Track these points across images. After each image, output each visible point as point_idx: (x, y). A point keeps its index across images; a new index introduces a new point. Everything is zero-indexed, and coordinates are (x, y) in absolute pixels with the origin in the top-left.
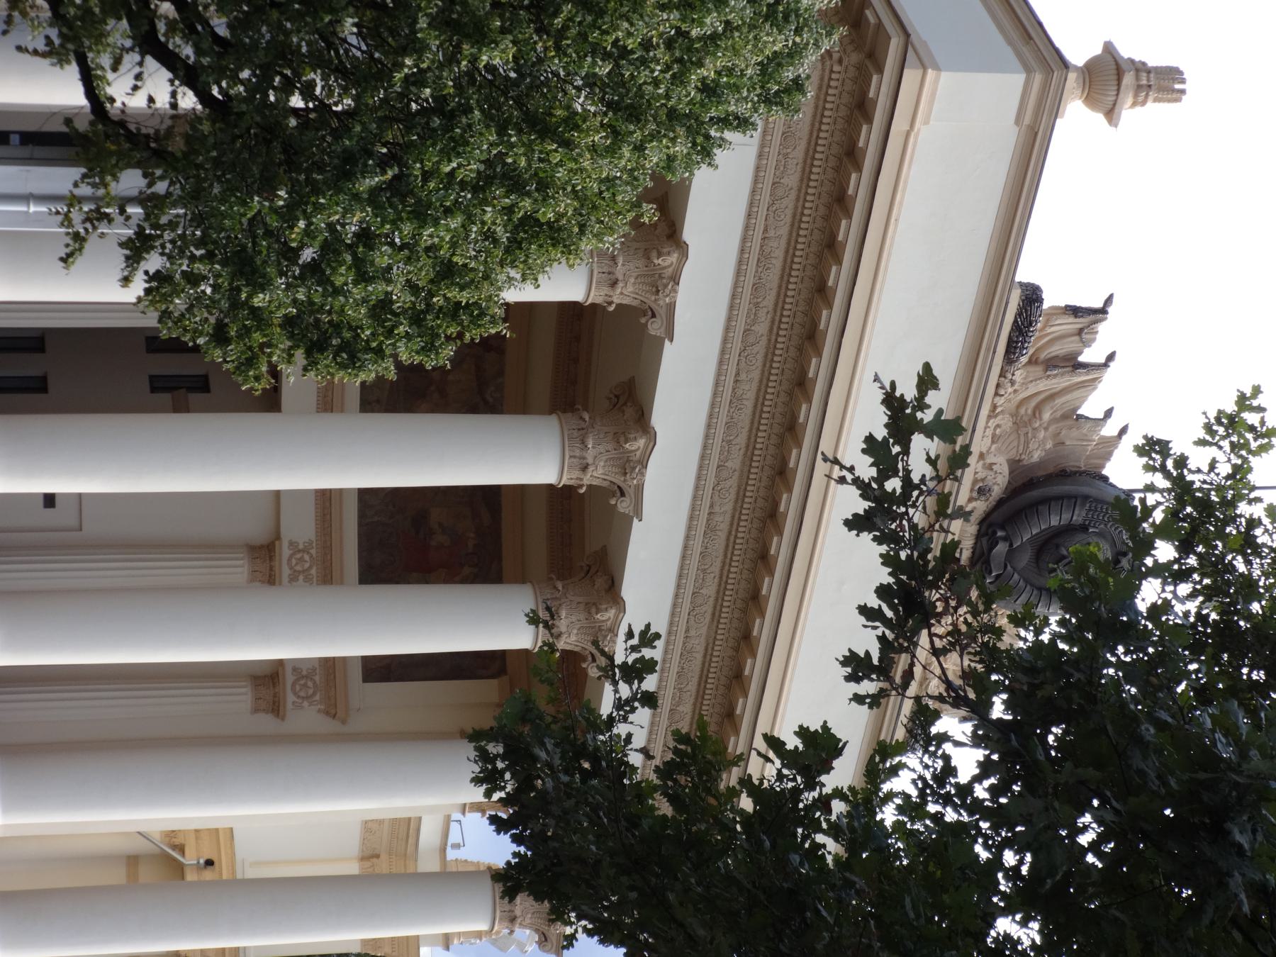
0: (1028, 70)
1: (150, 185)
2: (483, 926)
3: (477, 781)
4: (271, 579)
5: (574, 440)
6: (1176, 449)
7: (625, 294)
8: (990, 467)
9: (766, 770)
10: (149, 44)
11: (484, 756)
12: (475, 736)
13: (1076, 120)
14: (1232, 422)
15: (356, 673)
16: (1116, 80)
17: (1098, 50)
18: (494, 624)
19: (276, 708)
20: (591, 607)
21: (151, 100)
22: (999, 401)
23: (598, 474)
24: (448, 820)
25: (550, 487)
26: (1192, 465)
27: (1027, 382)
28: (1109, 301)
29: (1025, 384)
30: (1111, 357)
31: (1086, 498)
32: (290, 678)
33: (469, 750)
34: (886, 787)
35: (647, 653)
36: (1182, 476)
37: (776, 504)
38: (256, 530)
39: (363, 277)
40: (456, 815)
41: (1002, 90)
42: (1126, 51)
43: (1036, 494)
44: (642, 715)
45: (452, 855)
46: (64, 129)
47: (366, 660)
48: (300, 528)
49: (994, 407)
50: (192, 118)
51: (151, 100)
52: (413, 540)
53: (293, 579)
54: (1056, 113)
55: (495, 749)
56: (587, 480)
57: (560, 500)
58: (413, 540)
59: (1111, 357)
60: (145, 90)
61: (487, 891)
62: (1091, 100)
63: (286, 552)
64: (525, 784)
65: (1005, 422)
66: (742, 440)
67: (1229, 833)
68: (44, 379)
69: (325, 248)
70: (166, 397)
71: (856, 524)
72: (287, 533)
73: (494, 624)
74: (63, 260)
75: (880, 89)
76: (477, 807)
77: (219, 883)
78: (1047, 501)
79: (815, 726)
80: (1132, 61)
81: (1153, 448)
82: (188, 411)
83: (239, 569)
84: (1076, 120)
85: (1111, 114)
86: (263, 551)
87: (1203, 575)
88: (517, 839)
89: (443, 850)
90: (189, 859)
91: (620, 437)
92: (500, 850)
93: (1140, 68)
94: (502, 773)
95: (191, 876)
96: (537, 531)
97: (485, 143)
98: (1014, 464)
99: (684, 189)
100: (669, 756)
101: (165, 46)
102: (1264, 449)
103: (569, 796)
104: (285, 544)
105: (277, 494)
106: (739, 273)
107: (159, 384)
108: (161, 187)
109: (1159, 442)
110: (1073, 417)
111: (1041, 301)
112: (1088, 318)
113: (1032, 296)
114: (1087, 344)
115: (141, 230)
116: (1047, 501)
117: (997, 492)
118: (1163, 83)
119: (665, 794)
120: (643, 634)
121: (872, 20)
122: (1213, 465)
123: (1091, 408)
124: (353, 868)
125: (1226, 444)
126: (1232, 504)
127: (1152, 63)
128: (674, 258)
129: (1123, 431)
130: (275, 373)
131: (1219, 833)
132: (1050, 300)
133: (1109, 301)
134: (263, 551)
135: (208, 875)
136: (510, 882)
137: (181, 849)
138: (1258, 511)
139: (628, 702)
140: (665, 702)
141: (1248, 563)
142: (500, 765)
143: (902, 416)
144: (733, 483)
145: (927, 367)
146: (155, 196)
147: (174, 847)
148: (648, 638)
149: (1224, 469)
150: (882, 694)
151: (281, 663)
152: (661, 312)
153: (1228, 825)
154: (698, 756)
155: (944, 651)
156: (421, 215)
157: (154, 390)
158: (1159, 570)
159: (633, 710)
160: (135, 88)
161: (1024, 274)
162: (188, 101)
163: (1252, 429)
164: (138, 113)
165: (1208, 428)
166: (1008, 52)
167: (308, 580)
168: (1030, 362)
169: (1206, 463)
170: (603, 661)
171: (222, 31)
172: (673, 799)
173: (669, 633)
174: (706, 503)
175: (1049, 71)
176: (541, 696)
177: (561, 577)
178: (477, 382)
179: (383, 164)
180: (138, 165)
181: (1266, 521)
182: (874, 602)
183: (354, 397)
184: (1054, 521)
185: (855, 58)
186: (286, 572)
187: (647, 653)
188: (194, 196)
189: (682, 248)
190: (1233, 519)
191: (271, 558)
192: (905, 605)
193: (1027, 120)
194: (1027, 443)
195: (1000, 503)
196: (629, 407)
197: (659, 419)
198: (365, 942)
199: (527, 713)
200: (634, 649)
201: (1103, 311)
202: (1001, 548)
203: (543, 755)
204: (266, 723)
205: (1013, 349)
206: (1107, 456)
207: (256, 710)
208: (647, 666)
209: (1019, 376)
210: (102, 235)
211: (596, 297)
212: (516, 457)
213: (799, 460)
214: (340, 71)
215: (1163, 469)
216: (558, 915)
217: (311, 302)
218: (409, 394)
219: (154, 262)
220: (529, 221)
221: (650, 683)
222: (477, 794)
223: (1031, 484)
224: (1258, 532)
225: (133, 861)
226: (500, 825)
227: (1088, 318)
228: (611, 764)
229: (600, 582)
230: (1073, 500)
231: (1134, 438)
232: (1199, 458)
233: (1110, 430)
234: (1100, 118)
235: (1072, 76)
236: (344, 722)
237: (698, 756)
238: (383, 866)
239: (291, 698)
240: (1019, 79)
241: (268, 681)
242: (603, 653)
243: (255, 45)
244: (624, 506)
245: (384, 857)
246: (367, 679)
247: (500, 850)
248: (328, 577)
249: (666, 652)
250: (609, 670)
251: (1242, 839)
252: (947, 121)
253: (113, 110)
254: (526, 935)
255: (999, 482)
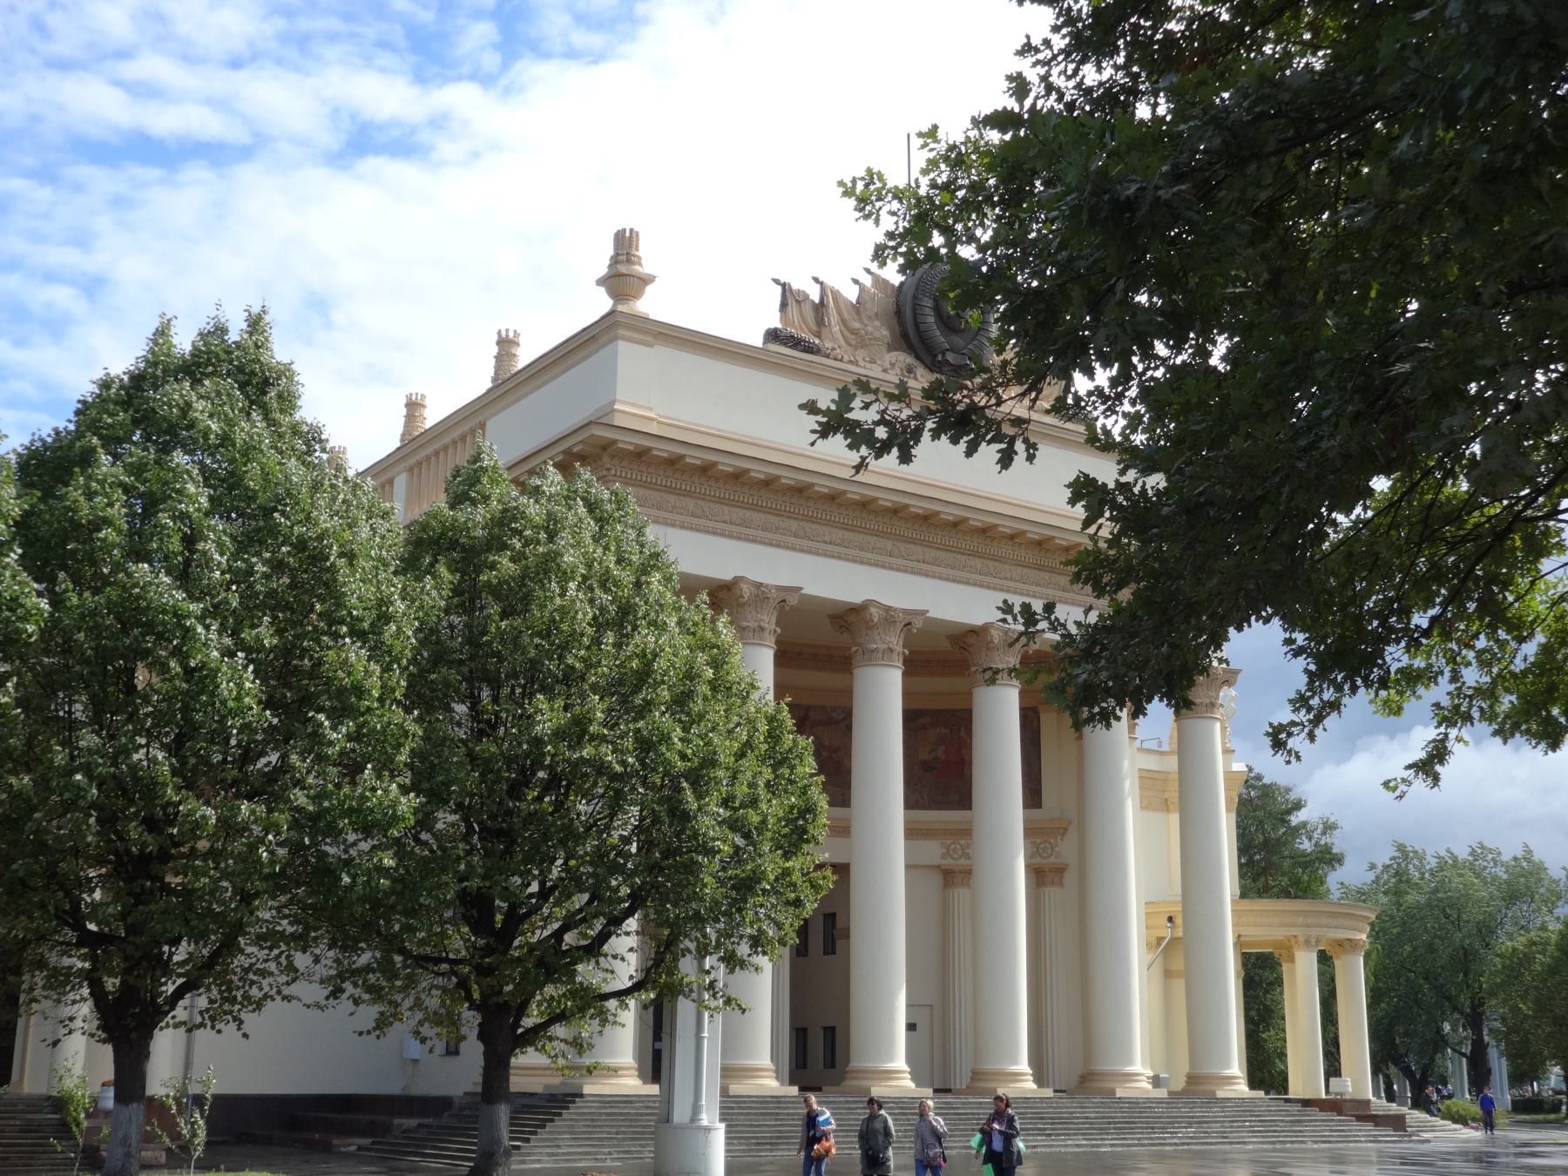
0: (615, 339)
1: (690, 952)
2: (1218, 725)
3: (1108, 726)
4: (968, 872)
5: (872, 657)
6: (881, 239)
7: (769, 621)
8: (893, 365)
9: (1106, 528)
10: (593, 949)
11: (1091, 719)
12: (1078, 726)
13: (650, 305)
14: (863, 201)
15: (1035, 812)
16: (623, 277)
17: (602, 290)
18: (1001, 712)
19: (1060, 870)
20: (989, 646)
21: (631, 950)
22: (846, 358)
23: (896, 641)
24: (1140, 750)
25: (904, 674)
26: (892, 228)
27: (834, 338)
28: (777, 281)
29: (834, 340)
30: (816, 280)
31: (915, 297)
32: (1039, 860)
33: (1087, 729)
34: (1118, 439)
35: (1017, 609)
36: (900, 235)
37: (917, 516)
38: (936, 880)
39: (753, 802)
40: (1137, 744)
41: (628, 354)
42: (603, 270)
43: (912, 332)
44: (1061, 612)
45: (1166, 748)
46: (651, 1009)
47: (1026, 806)
48: (932, 851)
49: (850, 362)
50: (645, 920)
51: (631, 950)
52: (941, 769)
53: (968, 856)
54: (646, 319)
55: (1085, 713)
56: (899, 648)
57: (915, 666)
58: (941, 769)
59: (816, 280)
60: (625, 955)
61: (1194, 724)
62: (638, 295)
63: (949, 861)
64: (1108, 692)
65: (861, 354)
66: (872, 540)
67: (1128, 198)
68: (826, 1029)
69: (733, 829)
70: (839, 943)
71: (906, 458)
72: (937, 861)
73: (1001, 712)
74: (744, 1011)
75: (627, 442)
76: (1132, 728)
77: (1185, 912)
78: (917, 324)
79: (1068, 493)
80: (610, 266)
81: (879, 254)
82: (848, 929)
83: (961, 894)
84: (650, 305)
85: (646, 280)
86: (949, 877)
87: (969, 219)
88: (1149, 701)
89: (1162, 753)
90: (1167, 934)
91: (869, 626)
92: (1158, 710)
93: (615, 260)
94: (1103, 709)
95: (1180, 933)
96: (940, 686)
97: (661, 718)
98: (891, 348)
99: (685, 577)
100: (1088, 588)
101: (594, 940)
102: (880, 177)
103: (1115, 661)
104: (944, 862)
105: (908, 867)
106: (754, 541)
107: (830, 948)
108: (692, 946)
109: (876, 251)
110: (858, 307)
111: (776, 330)
112: (789, 297)
113: (773, 336)
114: (806, 296)
115: (721, 959)
116: (917, 324)
117: (910, 360)
118: (625, 244)
119: (1116, 592)
120: (1004, 612)
121: (580, 447)
122: (894, 214)
123: (852, 294)
124: (1174, 818)
125: (878, 204)
126: (919, 200)
127: (611, 252)
128: (745, 587)
129: (868, 271)
130: (820, 867)
131: (1130, 205)
132: (775, 322)
133: (777, 281)
134: (949, 877)
135: (1179, 921)
136: (1182, 705)
137: (1160, 940)
138: (924, 182)
139: (1051, 623)
140: (1053, 594)
141: (961, 187)
142: (1097, 710)
143: (834, 423)
144: (902, 546)
145: (802, 407)
146: (698, 948)
147: (1159, 944)
148: (1007, 608)
149: (895, 205)
150: (1026, 441)
151: (1028, 867)
152: (782, 596)
153: (1122, 198)
154: (1091, 570)
155: (999, 398)
156: (710, 762)
157: (834, 953)
158: (951, 246)
159: (1057, 619)
160: (623, 959)
161: (758, 341)
162: (632, 924)
163: (866, 186)
164: (643, 959)
165: (867, 217)
166: (602, 352)
167: (968, 846)
168: (819, 337)
169: (892, 217)
170: (1024, 640)
171: (586, 897)
172: (1120, 586)
173: (1002, 590)
174: (916, 564)
175: (616, 325)
176: (1045, 679)
177: (968, 668)
178: (828, 726)
179: (679, 790)
180: (676, 960)
181: (932, 175)
182: (962, 446)
183: (840, 812)
184: (931, 319)
185: (606, 459)
186: (963, 861)
187: (1017, 609)
188: (699, 920)
189: (737, 580)
190: (929, 198)
191: (953, 872)
192: (964, 425)
193: (650, 339)
194: (876, 339)
195: (918, 358)
196: (849, 620)
197: (856, 598)
198: (1228, 810)
199: (1058, 689)
200: (1015, 619)
201: (784, 285)
202: (950, 357)
203: (1084, 676)
204: (1070, 877)
205: (809, 349)
206: (886, 282)
207: (1061, 884)
208: (1026, 608)
209: (828, 345)
210: (725, 985)
211: (771, 641)
212: (883, 700)
213: (855, 492)
214: (612, 816)
215: (894, 248)
216: (1205, 670)
217: (772, 839)
218: (837, 771)
219: (743, 950)
220: (714, 686)
221: (1038, 606)
222: (1121, 726)
223: (905, 336)
224: (939, 181)
225: (1168, 974)
226: (1138, 712)
227: (789, 297)
228: (1095, 635)
229: (972, 640)
230: (916, 306)
231: (874, 267)
232: (888, 223)
233: (867, 281)
234: (649, 289)
235: (620, 308)
236: (1070, 822)
237: (1091, 570)
238: (1173, 795)
239: (1052, 860)
240: (621, 343)
241: (1040, 876)
242: (1017, 640)
243: (594, 875)
244: (918, 623)
245: (1166, 795)
246: (1039, 806)
247: (1158, 710)
248: (966, 832)
249: (1015, 593)
250: (1029, 635)
251: (1134, 188)
252: (651, 399)
253: (638, 977)
254: (1227, 694)
255: (904, 359)
